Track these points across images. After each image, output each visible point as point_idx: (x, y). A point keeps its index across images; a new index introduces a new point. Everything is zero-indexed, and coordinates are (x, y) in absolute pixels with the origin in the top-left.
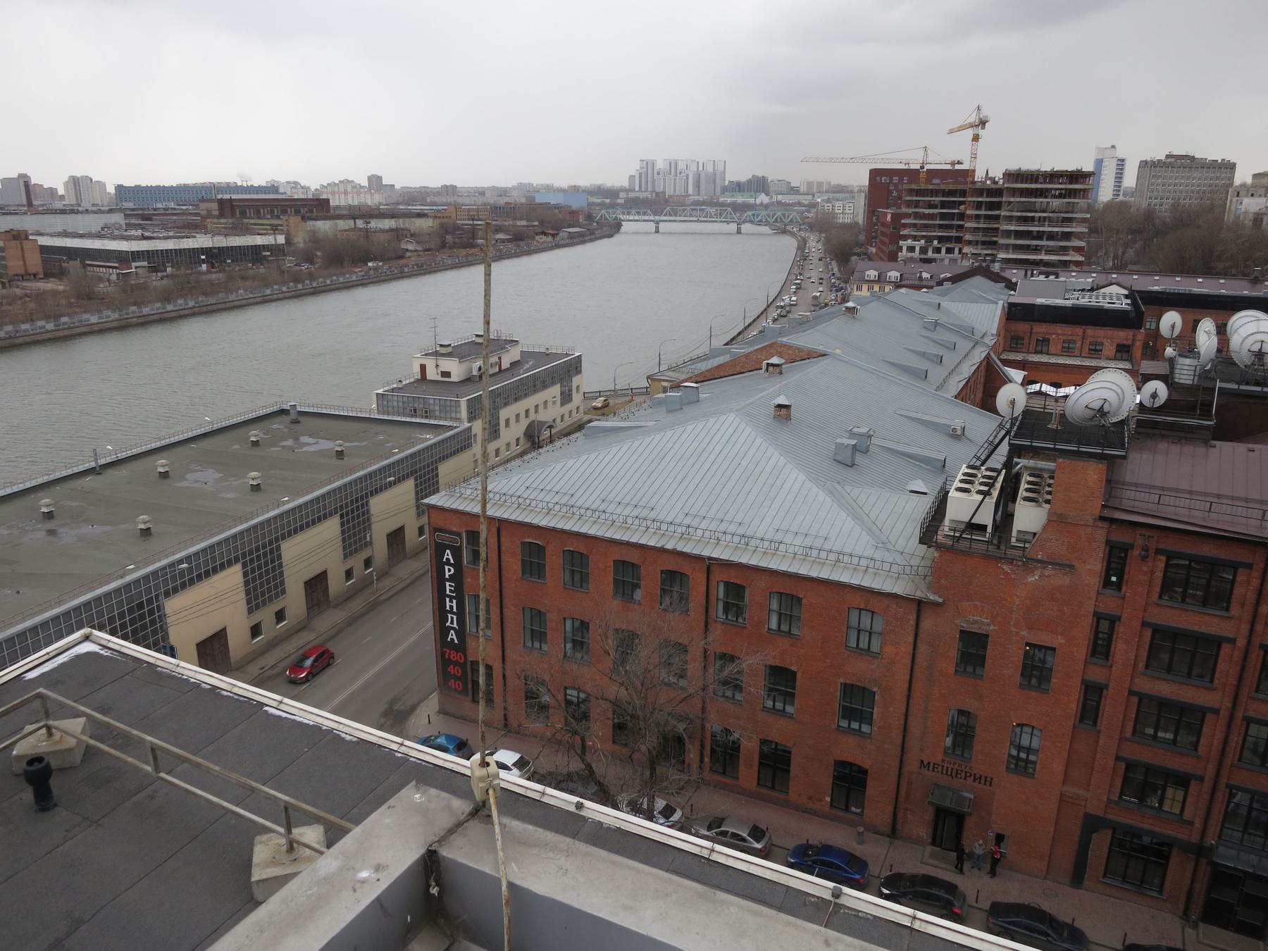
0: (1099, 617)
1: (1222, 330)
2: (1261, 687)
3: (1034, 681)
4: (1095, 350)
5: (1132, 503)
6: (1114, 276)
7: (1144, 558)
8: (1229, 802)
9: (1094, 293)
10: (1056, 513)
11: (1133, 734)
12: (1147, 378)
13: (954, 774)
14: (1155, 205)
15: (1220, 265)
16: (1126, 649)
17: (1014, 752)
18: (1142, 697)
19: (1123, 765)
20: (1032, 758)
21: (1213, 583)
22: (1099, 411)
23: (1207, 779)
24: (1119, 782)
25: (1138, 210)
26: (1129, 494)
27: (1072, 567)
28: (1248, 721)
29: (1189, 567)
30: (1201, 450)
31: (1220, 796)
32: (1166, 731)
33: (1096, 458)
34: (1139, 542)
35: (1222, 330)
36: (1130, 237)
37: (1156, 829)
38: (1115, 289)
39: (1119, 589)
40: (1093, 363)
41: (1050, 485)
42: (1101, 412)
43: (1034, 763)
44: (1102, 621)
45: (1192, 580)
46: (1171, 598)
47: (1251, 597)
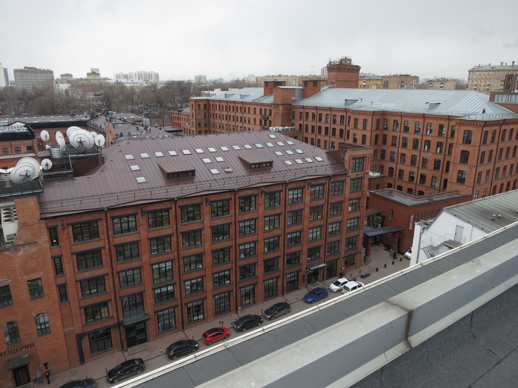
0: (54, 258)
1: (65, 136)
2: (118, 259)
3: (36, 295)
4: (18, 150)
5: (52, 209)
6: (17, 118)
7: (63, 229)
8: (122, 303)
9: (10, 126)
10: (21, 223)
11: (82, 296)
12: (42, 158)
13: (15, 351)
14: (26, 88)
15: (58, 110)
16: (69, 266)
17: (39, 327)
18: (81, 281)
19: (83, 310)
20: (47, 326)
21: (91, 229)
22: (26, 176)
23: (112, 299)
24: (84, 316)
25: (19, 90)
26: (49, 206)
27: (36, 242)
28: (118, 273)
29: (81, 227)
30: (71, 182)
31: (119, 303)
32: (93, 289)
33: (31, 195)
34: (59, 223)
35: (65, 136)
36: (19, 102)
37: (103, 326)
38: (18, 124)
39: (58, 244)
40: (19, 156)
41: (15, 212)
42: (27, 176)
43: (49, 327)
44: (56, 259)
45: (83, 231)
46: (79, 241)
47: (105, 230)
